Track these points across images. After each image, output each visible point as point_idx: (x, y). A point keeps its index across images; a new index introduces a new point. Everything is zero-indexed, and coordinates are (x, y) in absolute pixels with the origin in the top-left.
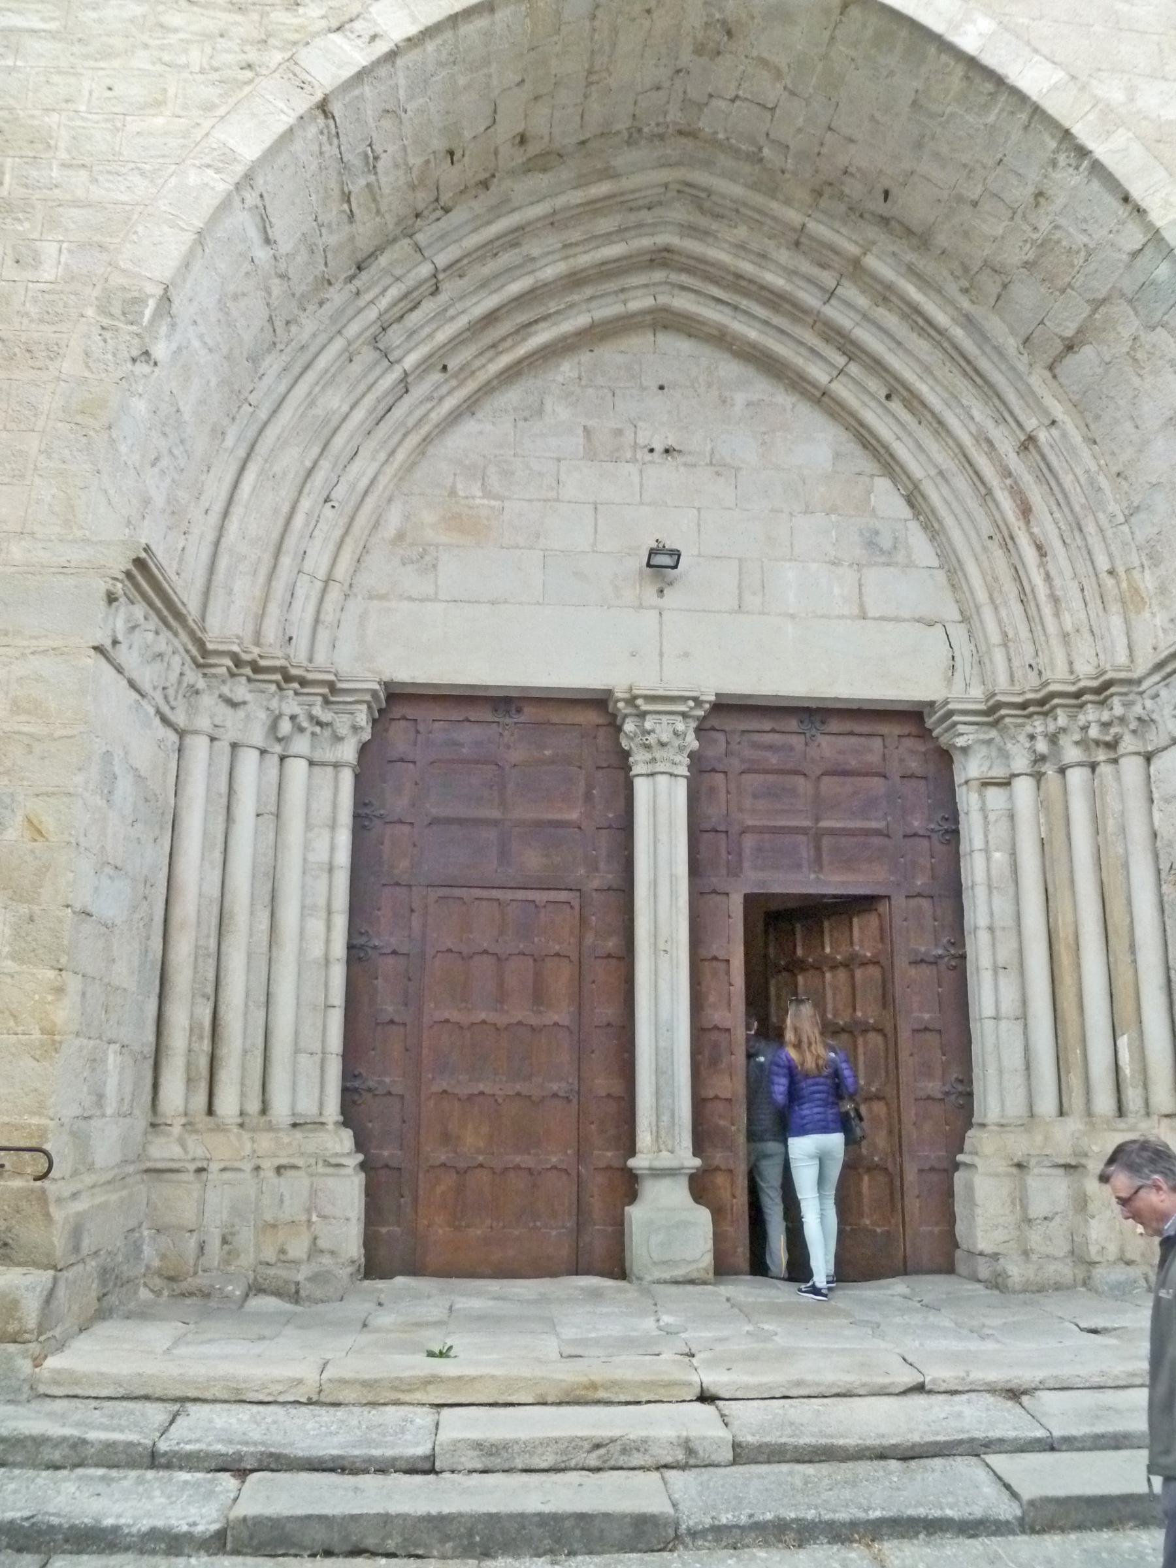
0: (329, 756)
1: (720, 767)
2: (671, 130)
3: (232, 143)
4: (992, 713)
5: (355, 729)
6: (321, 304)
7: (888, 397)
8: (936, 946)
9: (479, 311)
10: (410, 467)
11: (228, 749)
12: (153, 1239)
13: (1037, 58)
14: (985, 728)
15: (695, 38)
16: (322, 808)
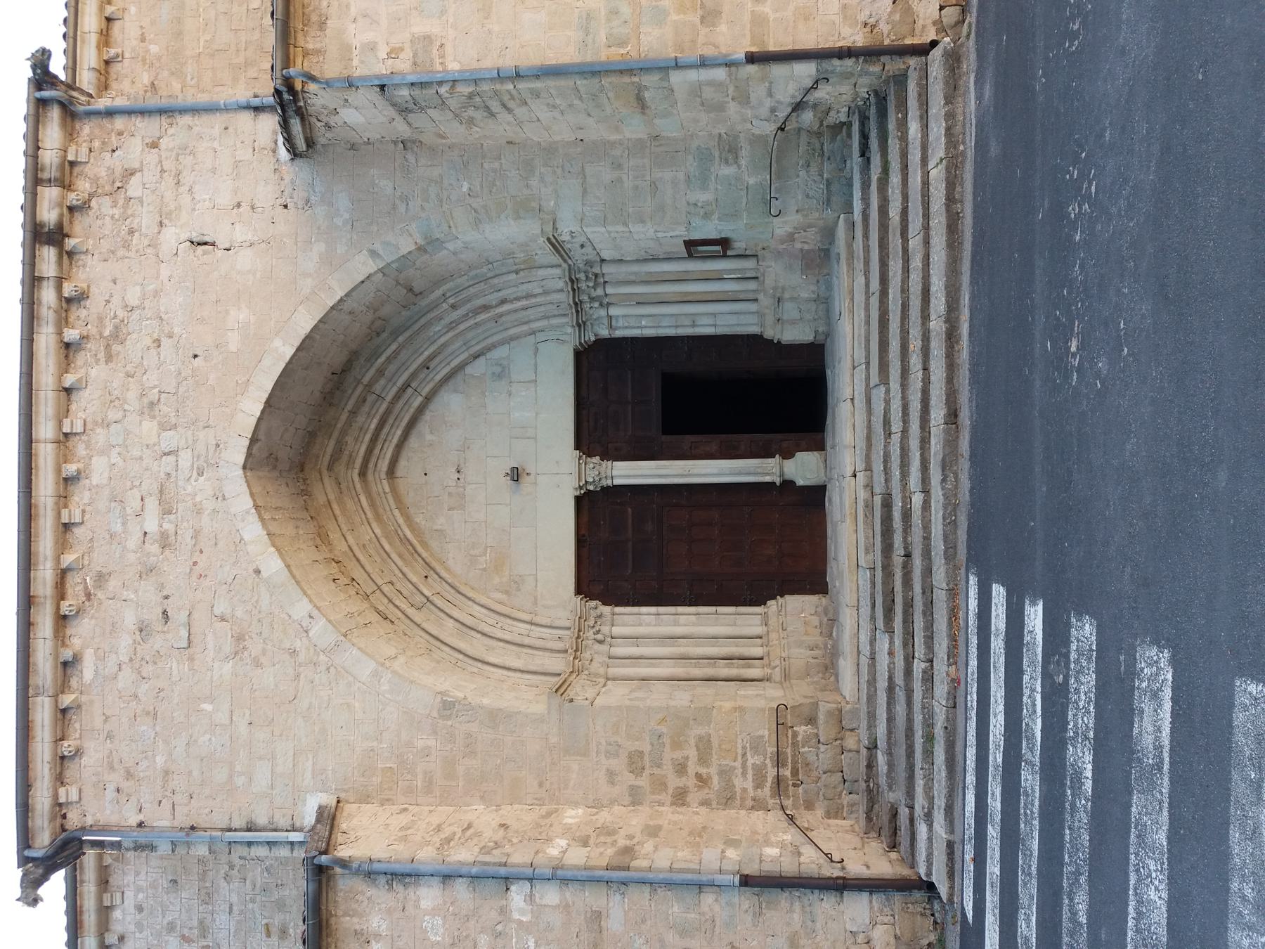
4: (580, 325)
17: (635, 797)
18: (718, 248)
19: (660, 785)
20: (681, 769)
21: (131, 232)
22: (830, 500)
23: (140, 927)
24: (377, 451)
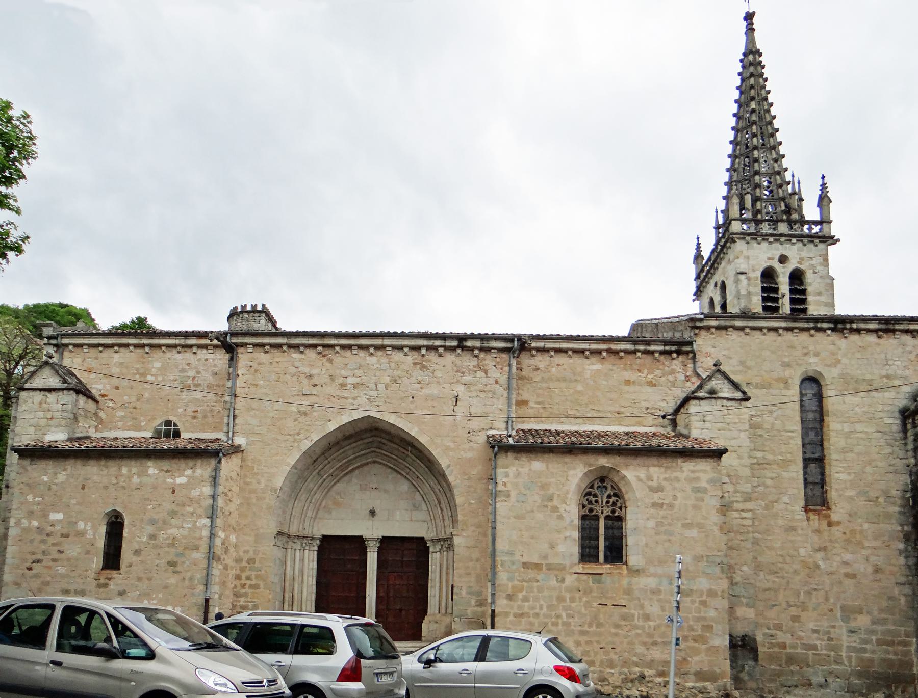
16: (311, 557)
17: (238, 560)
19: (243, 569)
20: (248, 578)
21: (463, 373)
23: (199, 360)
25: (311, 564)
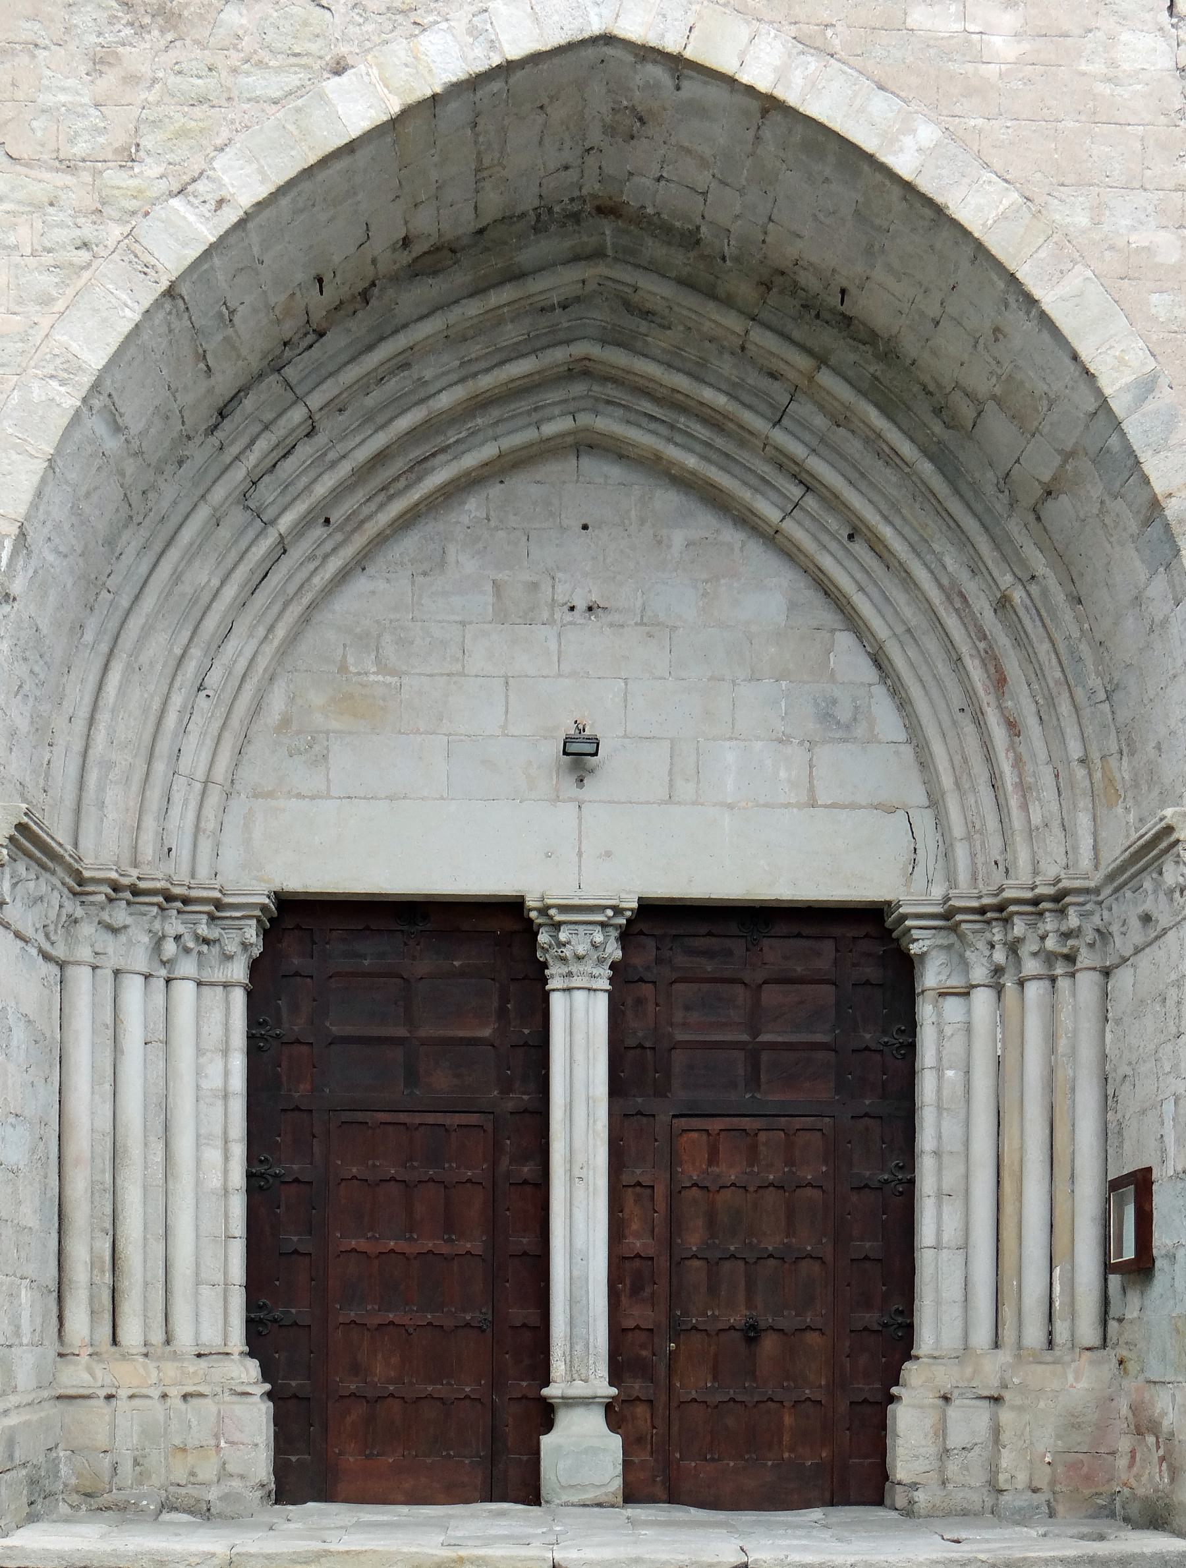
0: (219, 975)
1: (648, 976)
2: (588, 207)
3: (74, 347)
5: (245, 946)
6: (180, 463)
7: (851, 537)
8: (883, 1171)
9: (363, 454)
10: (294, 637)
11: (110, 977)
12: (69, 1459)
13: (988, 175)
14: (943, 933)
15: (603, 120)
18: (1129, 1253)
22: (502, 1514)
24: (648, 407)
25: (214, 1069)
